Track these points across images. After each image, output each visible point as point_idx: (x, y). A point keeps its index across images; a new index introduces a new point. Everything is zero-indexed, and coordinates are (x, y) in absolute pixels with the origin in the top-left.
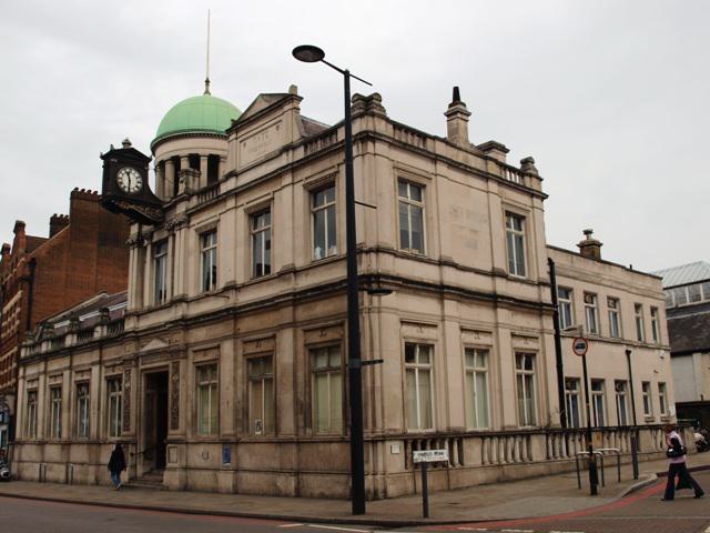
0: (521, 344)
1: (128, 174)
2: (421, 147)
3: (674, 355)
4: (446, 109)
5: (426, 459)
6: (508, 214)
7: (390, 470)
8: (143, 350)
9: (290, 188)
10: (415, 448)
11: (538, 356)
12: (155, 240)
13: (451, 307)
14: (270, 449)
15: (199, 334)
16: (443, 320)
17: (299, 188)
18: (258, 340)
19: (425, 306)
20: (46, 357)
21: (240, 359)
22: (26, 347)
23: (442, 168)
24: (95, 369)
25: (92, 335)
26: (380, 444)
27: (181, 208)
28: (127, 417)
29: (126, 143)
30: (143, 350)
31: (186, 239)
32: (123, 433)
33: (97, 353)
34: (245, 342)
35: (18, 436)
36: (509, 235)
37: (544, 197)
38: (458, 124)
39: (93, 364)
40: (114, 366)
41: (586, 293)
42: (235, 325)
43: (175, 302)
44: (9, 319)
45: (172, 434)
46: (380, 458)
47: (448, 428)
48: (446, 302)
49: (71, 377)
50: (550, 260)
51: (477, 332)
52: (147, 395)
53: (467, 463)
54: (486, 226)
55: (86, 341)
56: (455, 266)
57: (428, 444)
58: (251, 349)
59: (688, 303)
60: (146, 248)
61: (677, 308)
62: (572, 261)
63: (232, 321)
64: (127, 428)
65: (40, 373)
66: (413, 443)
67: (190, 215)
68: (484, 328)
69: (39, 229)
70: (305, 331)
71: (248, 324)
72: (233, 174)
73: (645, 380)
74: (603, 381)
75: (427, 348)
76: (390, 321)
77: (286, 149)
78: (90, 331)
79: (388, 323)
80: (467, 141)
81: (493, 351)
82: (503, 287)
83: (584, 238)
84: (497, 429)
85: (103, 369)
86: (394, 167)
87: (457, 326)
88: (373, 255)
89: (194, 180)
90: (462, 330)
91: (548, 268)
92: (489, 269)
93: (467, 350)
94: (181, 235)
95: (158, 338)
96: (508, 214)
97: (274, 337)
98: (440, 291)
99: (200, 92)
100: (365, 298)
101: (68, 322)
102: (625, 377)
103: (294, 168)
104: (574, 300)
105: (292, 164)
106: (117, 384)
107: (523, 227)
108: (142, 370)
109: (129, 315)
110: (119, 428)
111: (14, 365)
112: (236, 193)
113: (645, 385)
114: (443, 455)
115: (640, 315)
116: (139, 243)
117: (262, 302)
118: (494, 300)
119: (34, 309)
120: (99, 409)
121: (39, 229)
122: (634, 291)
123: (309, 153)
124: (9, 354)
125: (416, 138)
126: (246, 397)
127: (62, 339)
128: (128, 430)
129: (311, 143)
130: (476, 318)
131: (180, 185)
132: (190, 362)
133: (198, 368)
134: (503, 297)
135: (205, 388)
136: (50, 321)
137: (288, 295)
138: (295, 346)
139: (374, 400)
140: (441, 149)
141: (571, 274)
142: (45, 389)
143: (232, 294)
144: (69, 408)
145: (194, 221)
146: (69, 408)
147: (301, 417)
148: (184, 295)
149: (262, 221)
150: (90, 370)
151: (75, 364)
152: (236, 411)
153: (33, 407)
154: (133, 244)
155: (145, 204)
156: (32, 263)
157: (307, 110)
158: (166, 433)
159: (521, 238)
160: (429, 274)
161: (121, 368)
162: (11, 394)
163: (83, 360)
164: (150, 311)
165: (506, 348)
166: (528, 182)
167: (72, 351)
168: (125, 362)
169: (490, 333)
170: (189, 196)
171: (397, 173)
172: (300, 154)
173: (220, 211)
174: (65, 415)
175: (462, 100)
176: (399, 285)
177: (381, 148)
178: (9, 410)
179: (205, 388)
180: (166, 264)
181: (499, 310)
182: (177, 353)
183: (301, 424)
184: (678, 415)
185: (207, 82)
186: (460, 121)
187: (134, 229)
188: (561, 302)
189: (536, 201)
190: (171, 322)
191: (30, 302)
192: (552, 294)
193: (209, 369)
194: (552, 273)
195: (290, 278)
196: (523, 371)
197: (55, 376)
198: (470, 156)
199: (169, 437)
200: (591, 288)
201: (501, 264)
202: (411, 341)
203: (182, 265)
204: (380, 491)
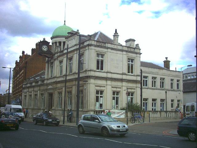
2: (104, 46)
3: (184, 92)
4: (113, 35)
13: (109, 82)
15: (59, 85)
19: (103, 82)
20: (28, 88)
22: (24, 84)
23: (109, 50)
24: (39, 91)
27: (56, 55)
33: (39, 87)
36: (129, 64)
37: (141, 54)
40: (42, 91)
43: (55, 77)
51: (116, 88)
52: (49, 98)
54: (121, 63)
55: (37, 84)
56: (111, 73)
77: (76, 45)
78: (38, 82)
80: (118, 42)
82: (124, 77)
83: (165, 59)
87: (111, 87)
88: (89, 72)
97: (72, 87)
98: (106, 79)
99: (62, 24)
102: (164, 98)
113: (172, 101)
116: (48, 62)
118: (122, 80)
121: (30, 53)
127: (32, 83)
137: (74, 78)
139: (87, 104)
144: (33, 100)
146: (33, 100)
156: (26, 63)
163: (36, 89)
164: (50, 79)
166: (136, 50)
167: (34, 87)
177: (92, 47)
185: (65, 21)
186: (116, 38)
187: (47, 59)
189: (138, 55)
191: (26, 72)
192: (147, 75)
194: (141, 73)
195: (75, 75)
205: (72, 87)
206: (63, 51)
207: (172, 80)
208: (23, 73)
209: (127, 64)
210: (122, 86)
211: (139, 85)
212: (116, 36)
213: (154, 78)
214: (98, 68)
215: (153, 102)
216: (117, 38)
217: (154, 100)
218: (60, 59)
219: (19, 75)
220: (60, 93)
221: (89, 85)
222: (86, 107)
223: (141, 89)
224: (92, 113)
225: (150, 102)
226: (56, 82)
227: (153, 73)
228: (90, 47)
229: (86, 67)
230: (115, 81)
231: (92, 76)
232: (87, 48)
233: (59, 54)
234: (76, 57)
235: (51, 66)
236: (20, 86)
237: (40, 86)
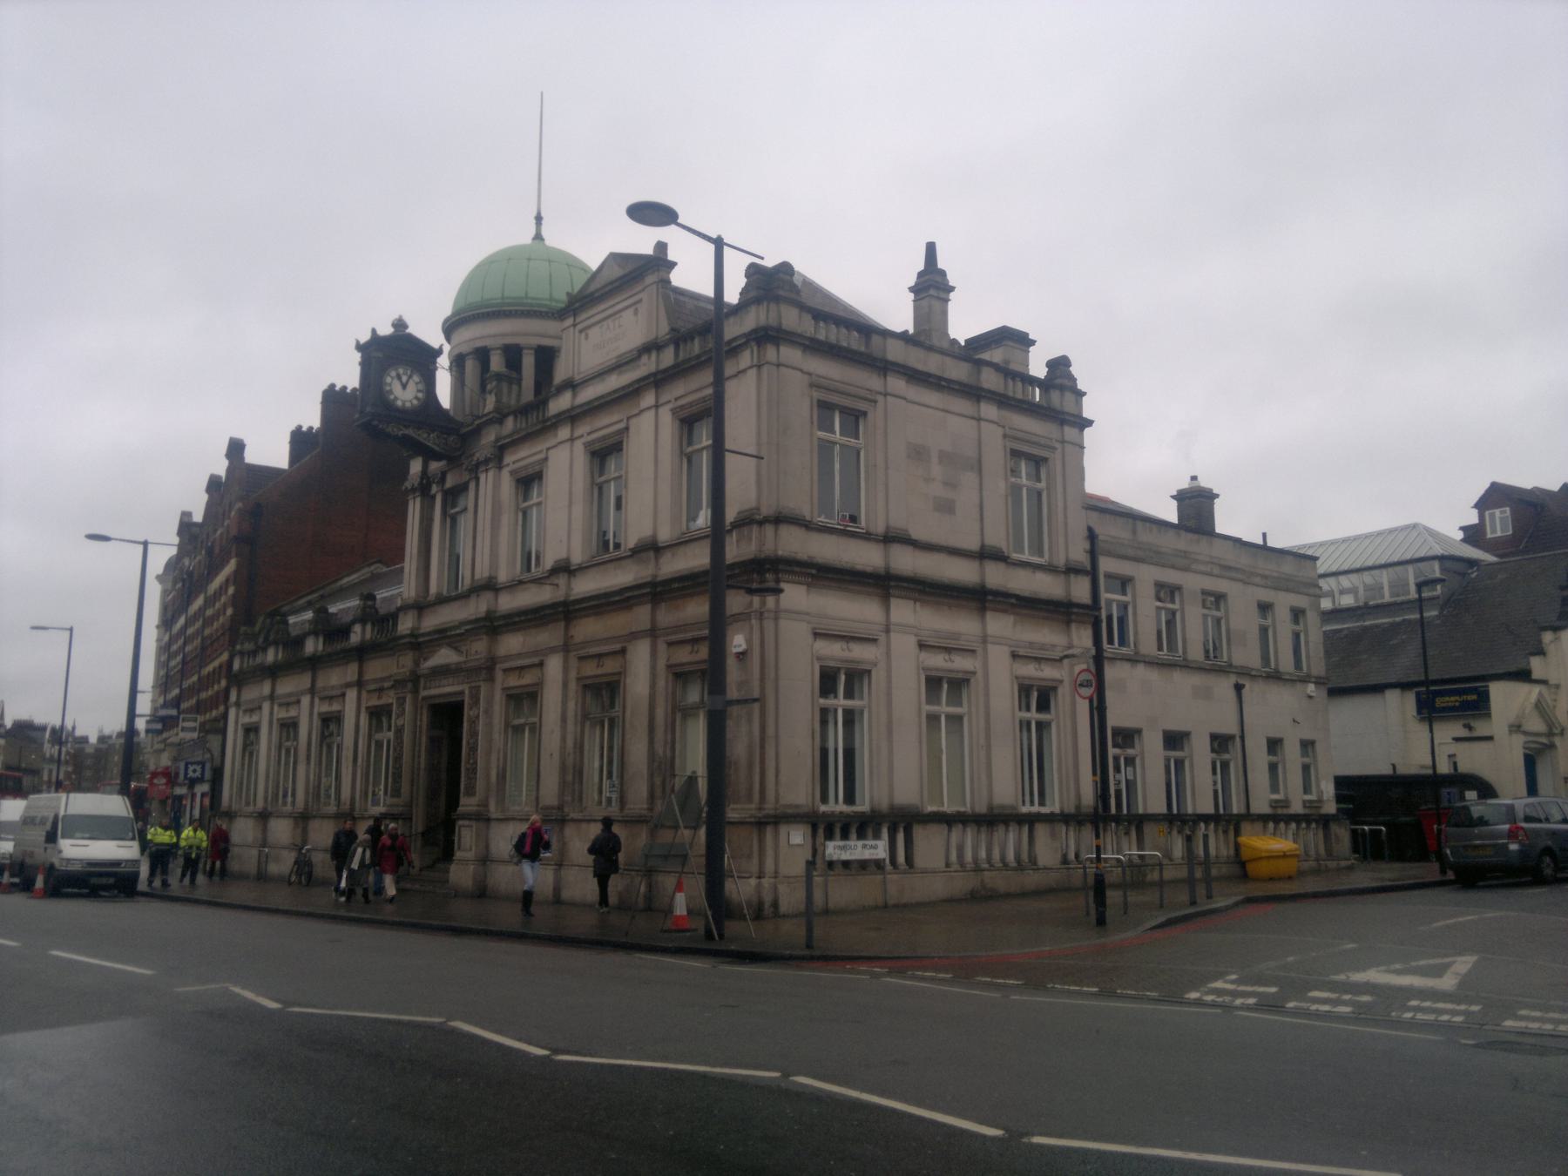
0: (1029, 670)
4: (912, 281)
5: (845, 856)
6: (1015, 454)
7: (785, 870)
9: (653, 412)
10: (829, 836)
11: (1060, 691)
12: (449, 483)
15: (512, 643)
16: (887, 631)
17: (666, 416)
18: (600, 656)
19: (859, 610)
20: (273, 672)
21: (573, 686)
22: (242, 653)
23: (896, 384)
25: (348, 638)
26: (769, 830)
27: (489, 437)
29: (400, 325)
31: (497, 486)
34: (581, 658)
39: (349, 685)
40: (381, 690)
41: (1160, 586)
42: (567, 628)
44: (217, 605)
45: (467, 804)
46: (770, 852)
47: (991, 808)
48: (894, 601)
50: (1090, 530)
52: (433, 741)
53: (919, 862)
55: (339, 646)
56: (982, 529)
58: (590, 669)
59: (1387, 599)
60: (433, 497)
61: (1366, 606)
62: (1134, 532)
63: (562, 624)
66: (826, 827)
67: (501, 449)
69: (270, 451)
70: (670, 644)
71: (588, 629)
73: (1272, 735)
74: (1186, 735)
75: (857, 677)
78: (345, 631)
82: (995, 576)
84: (982, 808)
86: (812, 385)
88: (769, 530)
90: (922, 646)
92: (973, 544)
94: (487, 479)
95: (449, 645)
96: (1015, 454)
97: (623, 651)
98: (883, 584)
102: (1231, 728)
103: (659, 380)
104: (1134, 596)
105: (654, 374)
106: (384, 720)
107: (1043, 476)
108: (424, 698)
112: (572, 417)
113: (1274, 745)
114: (878, 849)
115: (1300, 627)
116: (424, 489)
117: (607, 595)
118: (980, 598)
121: (270, 451)
122: (1257, 580)
123: (682, 356)
124: (216, 663)
125: (844, 331)
126: (580, 747)
127: (299, 642)
129: (685, 341)
133: (509, 697)
135: (518, 730)
136: (285, 609)
138: (653, 668)
140: (895, 352)
141: (1131, 552)
143: (562, 580)
145: (509, 459)
149: (612, 464)
152: (563, 769)
153: (251, 754)
154: (413, 490)
157: (678, 278)
158: (457, 804)
159: (1039, 494)
160: (867, 557)
161: (392, 693)
163: (334, 678)
164: (442, 600)
165: (999, 679)
169: (973, 651)
170: (499, 417)
171: (817, 395)
172: (668, 358)
173: (548, 444)
178: (212, 759)
179: (518, 730)
180: (465, 523)
182: (489, 667)
184: (1340, 798)
185: (539, 219)
188: (1109, 602)
189: (1070, 432)
190: (470, 622)
193: (524, 699)
194: (1093, 554)
196: (1034, 715)
197: (288, 704)
198: (948, 360)
200: (1171, 576)
201: (997, 537)
202: (832, 664)
203: (488, 526)
204: (767, 905)
206: (540, 403)
207: (1265, 608)
208: (235, 578)
210: (984, 640)
216: (936, 304)
221: (769, 625)
222: (750, 789)
232: (746, 359)
235: (444, 513)
237: (361, 661)
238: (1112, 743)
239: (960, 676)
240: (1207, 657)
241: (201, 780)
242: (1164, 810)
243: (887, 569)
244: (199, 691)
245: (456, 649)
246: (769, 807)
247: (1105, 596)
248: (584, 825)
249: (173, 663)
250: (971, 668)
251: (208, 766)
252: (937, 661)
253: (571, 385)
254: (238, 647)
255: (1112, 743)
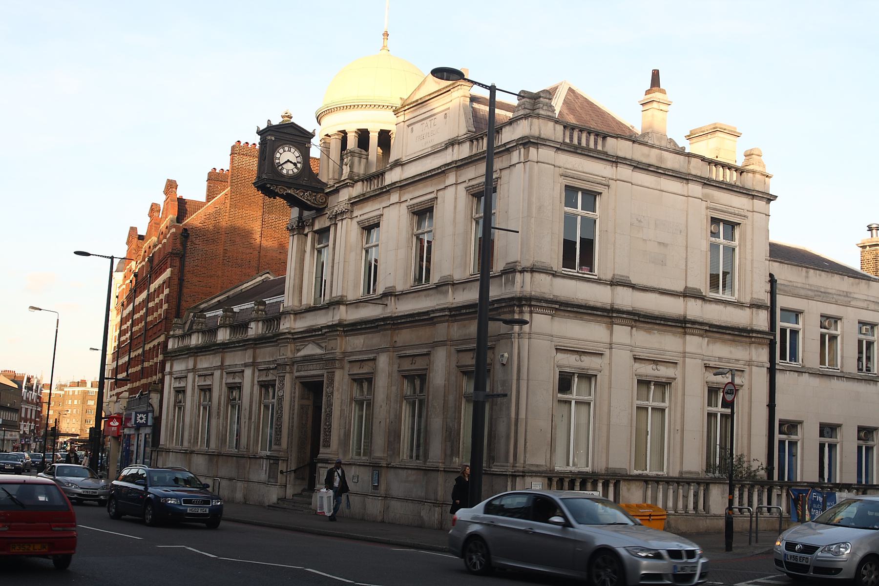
1: (295, 164)
2: (600, 148)
6: (715, 221)
8: (300, 354)
11: (740, 393)
13: (622, 333)
14: (413, 476)
16: (611, 348)
19: (592, 332)
23: (624, 172)
24: (248, 372)
25: (246, 331)
27: (345, 195)
28: (279, 431)
30: (300, 354)
32: (274, 447)
33: (250, 352)
35: (162, 441)
36: (714, 247)
37: (770, 199)
38: (653, 116)
39: (246, 365)
40: (268, 369)
49: (222, 378)
50: (771, 275)
51: (655, 362)
52: (302, 407)
55: (239, 337)
56: (633, 287)
57: (578, 484)
58: (407, 365)
60: (306, 235)
64: (278, 442)
65: (188, 371)
68: (667, 357)
71: (405, 336)
72: (398, 164)
76: (542, 346)
77: (453, 143)
78: (245, 326)
79: (540, 347)
81: (677, 384)
82: (694, 310)
84: (675, 473)
85: (257, 373)
88: (528, 276)
89: (360, 162)
90: (636, 359)
91: (768, 287)
92: (680, 288)
93: (640, 382)
97: (428, 354)
100: (495, 327)
101: (220, 312)
108: (297, 377)
109: (286, 313)
110: (271, 441)
111: (161, 357)
118: (682, 325)
119: (185, 290)
120: (250, 418)
124: (155, 342)
127: (213, 331)
128: (280, 445)
130: (657, 346)
131: (344, 167)
132: (346, 373)
134: (694, 322)
141: (802, 292)
142: (193, 389)
144: (219, 413)
146: (219, 413)
147: (449, 444)
148: (342, 296)
150: (243, 371)
151: (227, 363)
155: (306, 188)
160: (600, 295)
161: (275, 372)
162: (156, 391)
163: (235, 359)
164: (310, 310)
165: (693, 385)
167: (225, 347)
168: (280, 366)
170: (353, 180)
174: (214, 422)
175: (663, 85)
176: (556, 309)
177: (545, 153)
181: (688, 337)
183: (449, 452)
185: (386, 34)
189: (759, 204)
191: (181, 280)
194: (773, 293)
199: (320, 456)
200: (832, 310)
205: (428, 354)
206: (380, 175)
208: (168, 283)
209: (704, 245)
211: (762, 355)
212: (655, 105)
213: (829, 320)
214: (568, 260)
215: (823, 439)
217: (828, 429)
218: (368, 211)
219: (144, 295)
220: (365, 381)
221: (525, 342)
222: (507, 452)
223: (772, 371)
224: (537, 486)
225: (808, 440)
226: (340, 324)
227: (821, 295)
228: (533, 150)
229: (506, 250)
230: (646, 330)
231: (539, 300)
232: (515, 157)
233: (358, 189)
234: (453, 204)
236: (147, 347)
238: (782, 430)
239: (664, 380)
240: (860, 370)
241: (145, 425)
242: (815, 479)
243: (612, 304)
244: (143, 361)
245: (318, 345)
246: (520, 466)
247: (779, 324)
248: (400, 471)
249: (123, 338)
250: (673, 376)
251: (150, 415)
252: (647, 370)
253: (398, 164)
254: (171, 333)
255: (782, 430)
